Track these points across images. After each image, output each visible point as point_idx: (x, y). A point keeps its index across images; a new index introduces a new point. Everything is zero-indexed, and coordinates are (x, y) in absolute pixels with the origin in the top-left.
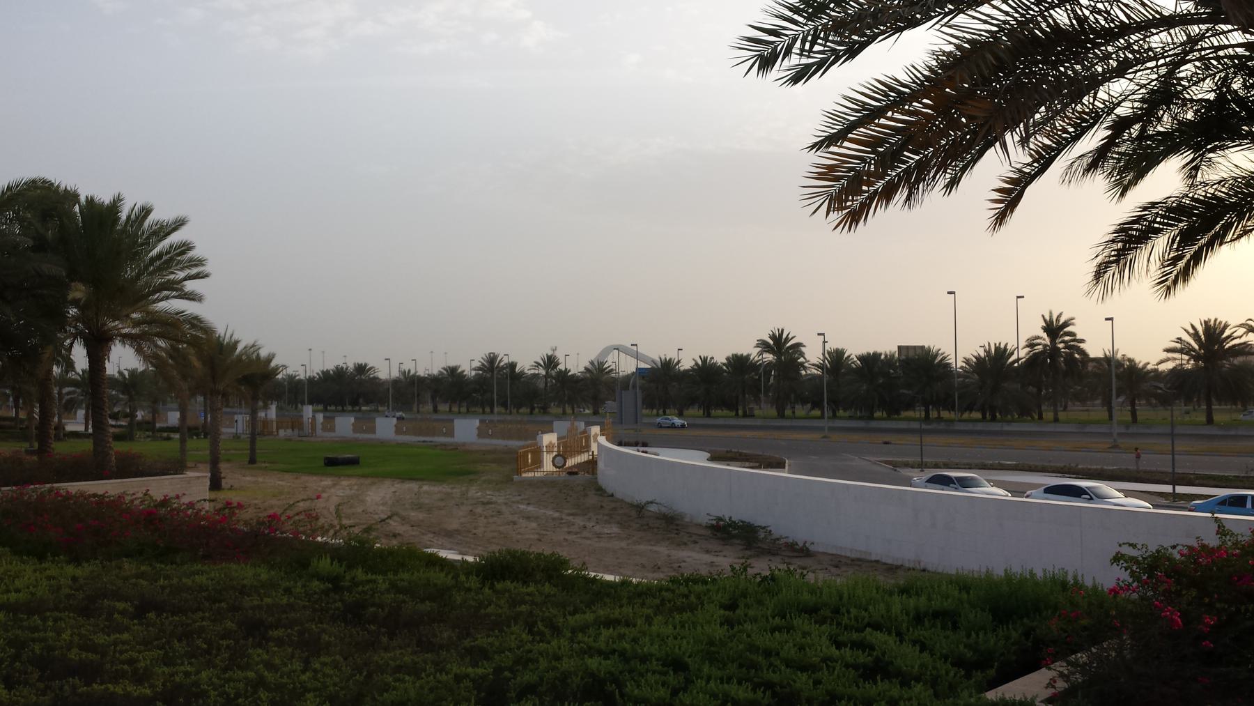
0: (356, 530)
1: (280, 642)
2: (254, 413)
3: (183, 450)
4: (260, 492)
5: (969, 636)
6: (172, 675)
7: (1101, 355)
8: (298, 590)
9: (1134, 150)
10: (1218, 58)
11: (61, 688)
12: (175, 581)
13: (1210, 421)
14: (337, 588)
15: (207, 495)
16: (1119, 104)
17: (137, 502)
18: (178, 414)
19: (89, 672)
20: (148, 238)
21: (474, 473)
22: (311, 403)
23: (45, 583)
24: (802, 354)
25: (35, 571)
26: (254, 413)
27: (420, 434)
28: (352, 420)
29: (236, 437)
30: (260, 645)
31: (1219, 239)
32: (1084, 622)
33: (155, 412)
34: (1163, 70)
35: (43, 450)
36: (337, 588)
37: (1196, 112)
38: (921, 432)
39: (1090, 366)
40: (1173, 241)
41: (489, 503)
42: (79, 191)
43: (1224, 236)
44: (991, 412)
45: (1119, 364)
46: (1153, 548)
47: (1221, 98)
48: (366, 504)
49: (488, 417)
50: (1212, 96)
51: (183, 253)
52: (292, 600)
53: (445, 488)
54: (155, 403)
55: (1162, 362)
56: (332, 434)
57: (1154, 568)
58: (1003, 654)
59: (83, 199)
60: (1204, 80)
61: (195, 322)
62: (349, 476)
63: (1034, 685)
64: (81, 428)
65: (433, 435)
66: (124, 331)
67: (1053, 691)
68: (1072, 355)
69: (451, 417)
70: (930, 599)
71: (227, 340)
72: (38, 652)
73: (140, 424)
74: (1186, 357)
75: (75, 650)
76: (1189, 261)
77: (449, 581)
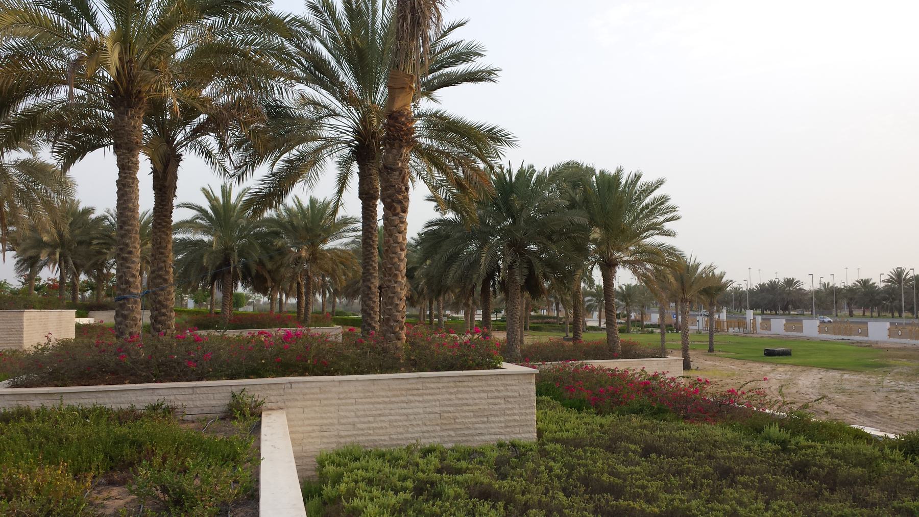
0: (795, 407)
1: (746, 486)
2: (710, 316)
3: (663, 341)
4: (721, 374)
6: (672, 500)
8: (756, 448)
11: (599, 500)
12: (667, 433)
14: (785, 450)
15: (682, 373)
17: (636, 376)
18: (658, 316)
19: (617, 492)
20: (639, 195)
21: (887, 366)
22: (751, 308)
23: (583, 426)
25: (577, 418)
26: (710, 316)
27: (839, 334)
28: (784, 321)
29: (699, 332)
30: (730, 486)
33: (643, 314)
35: (576, 338)
36: (785, 450)
41: (901, 391)
42: (595, 167)
48: (797, 386)
49: (897, 321)
51: (662, 203)
52: (752, 455)
53: (863, 377)
54: (643, 307)
56: (799, 334)
59: (598, 173)
61: (671, 251)
62: (785, 364)
64: (596, 324)
65: (850, 335)
66: (624, 259)
69: (864, 320)
71: (692, 263)
72: (583, 473)
73: (633, 321)
75: (606, 475)
77: (877, 452)
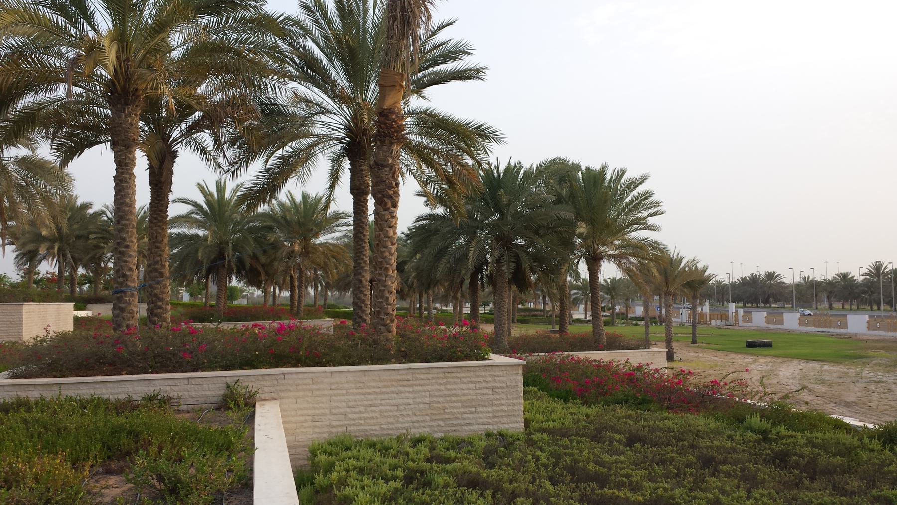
0: (776, 398)
1: (728, 474)
2: (693, 309)
3: (647, 333)
4: (703, 365)
6: (656, 489)
8: (738, 437)
11: (585, 488)
12: (651, 423)
14: (766, 439)
15: (666, 364)
17: (621, 367)
18: (642, 308)
19: (602, 480)
20: (624, 190)
21: (866, 357)
22: (733, 301)
23: (569, 416)
25: (563, 408)
26: (693, 309)
27: (819, 326)
28: (765, 314)
29: (682, 324)
30: (713, 475)
33: (627, 307)
35: (562, 330)
36: (766, 439)
41: (879, 382)
42: (581, 163)
48: (778, 377)
49: (875, 313)
51: (647, 198)
52: (734, 444)
53: (842, 368)
54: (628, 300)
56: (780, 326)
59: (583, 169)
61: (655, 245)
62: (766, 356)
64: (582, 317)
65: (830, 327)
66: (609, 253)
69: (843, 312)
71: (675, 257)
72: (569, 462)
73: (618, 314)
75: (591, 464)
77: (856, 442)
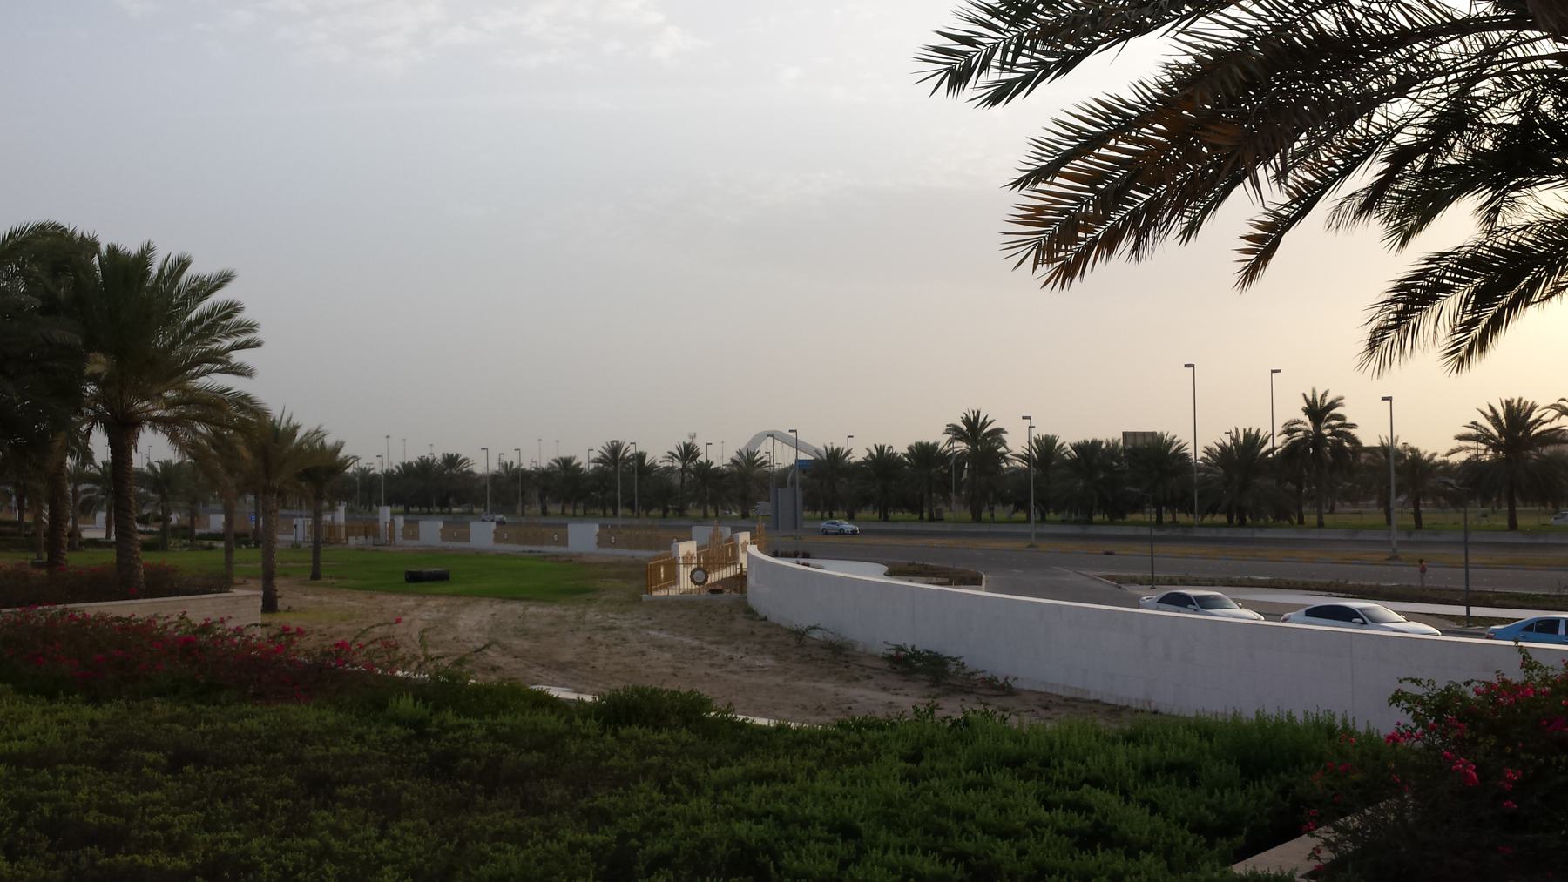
0: (446, 662)
1: (350, 802)
2: (317, 516)
3: (229, 562)
4: (325, 615)
5: (1211, 794)
6: (215, 843)
7: (1377, 444)
8: (373, 737)
9: (1418, 187)
10: (1523, 73)
11: (76, 860)
12: (219, 726)
13: (1513, 526)
14: (422, 735)
15: (259, 619)
16: (1399, 130)
17: (171, 627)
18: (222, 518)
19: (111, 840)
20: (185, 297)
21: (593, 591)
22: (389, 503)
23: (56, 728)
24: (1003, 443)
25: (44, 713)
26: (317, 516)
27: (525, 543)
28: (441, 524)
29: (296, 546)
30: (325, 806)
31: (1525, 298)
32: (1356, 777)
33: (193, 515)
34: (1455, 88)
35: (54, 562)
36: (422, 735)
37: (1495, 140)
38: (1151, 540)
39: (1363, 458)
40: (1467, 301)
41: (611, 628)
42: (99, 239)
43: (1531, 295)
44: (1239, 515)
45: (1400, 455)
46: (1441, 685)
47: (1526, 122)
48: (458, 630)
49: (610, 521)
50: (1515, 120)
51: (229, 316)
52: (365, 749)
53: (557, 610)
54: (194, 504)
55: (1453, 452)
56: (416, 543)
57: (1443, 709)
58: (1254, 817)
59: (103, 249)
60: (1505, 100)
61: (244, 402)
62: (437, 595)
63: (1293, 856)
64: (101, 535)
65: (542, 543)
66: (155, 414)
67: (1317, 863)
68: (1340, 443)
69: (564, 521)
70: (1162, 749)
71: (284, 424)
72: (47, 814)
73: (175, 530)
74: (1482, 446)
75: (94, 813)
76: (1486, 326)
77: (562, 726)
